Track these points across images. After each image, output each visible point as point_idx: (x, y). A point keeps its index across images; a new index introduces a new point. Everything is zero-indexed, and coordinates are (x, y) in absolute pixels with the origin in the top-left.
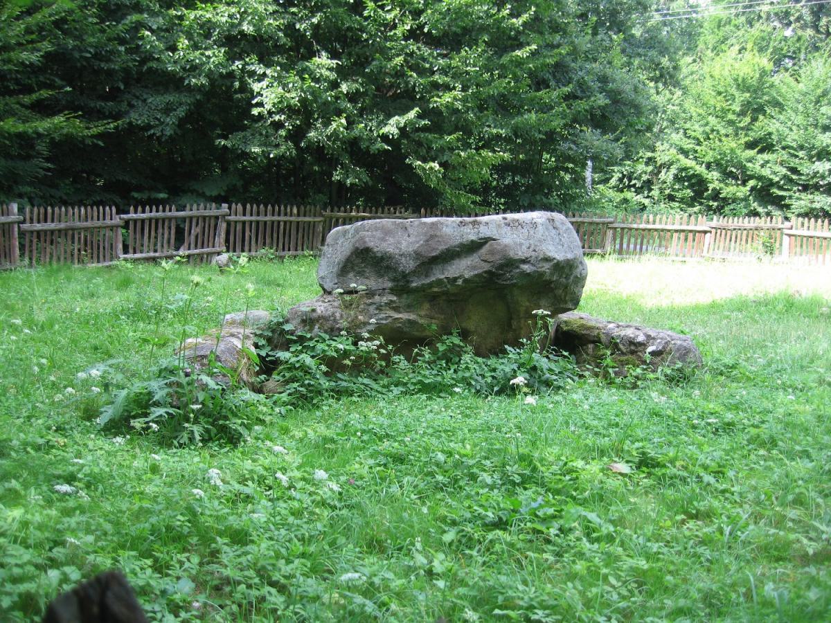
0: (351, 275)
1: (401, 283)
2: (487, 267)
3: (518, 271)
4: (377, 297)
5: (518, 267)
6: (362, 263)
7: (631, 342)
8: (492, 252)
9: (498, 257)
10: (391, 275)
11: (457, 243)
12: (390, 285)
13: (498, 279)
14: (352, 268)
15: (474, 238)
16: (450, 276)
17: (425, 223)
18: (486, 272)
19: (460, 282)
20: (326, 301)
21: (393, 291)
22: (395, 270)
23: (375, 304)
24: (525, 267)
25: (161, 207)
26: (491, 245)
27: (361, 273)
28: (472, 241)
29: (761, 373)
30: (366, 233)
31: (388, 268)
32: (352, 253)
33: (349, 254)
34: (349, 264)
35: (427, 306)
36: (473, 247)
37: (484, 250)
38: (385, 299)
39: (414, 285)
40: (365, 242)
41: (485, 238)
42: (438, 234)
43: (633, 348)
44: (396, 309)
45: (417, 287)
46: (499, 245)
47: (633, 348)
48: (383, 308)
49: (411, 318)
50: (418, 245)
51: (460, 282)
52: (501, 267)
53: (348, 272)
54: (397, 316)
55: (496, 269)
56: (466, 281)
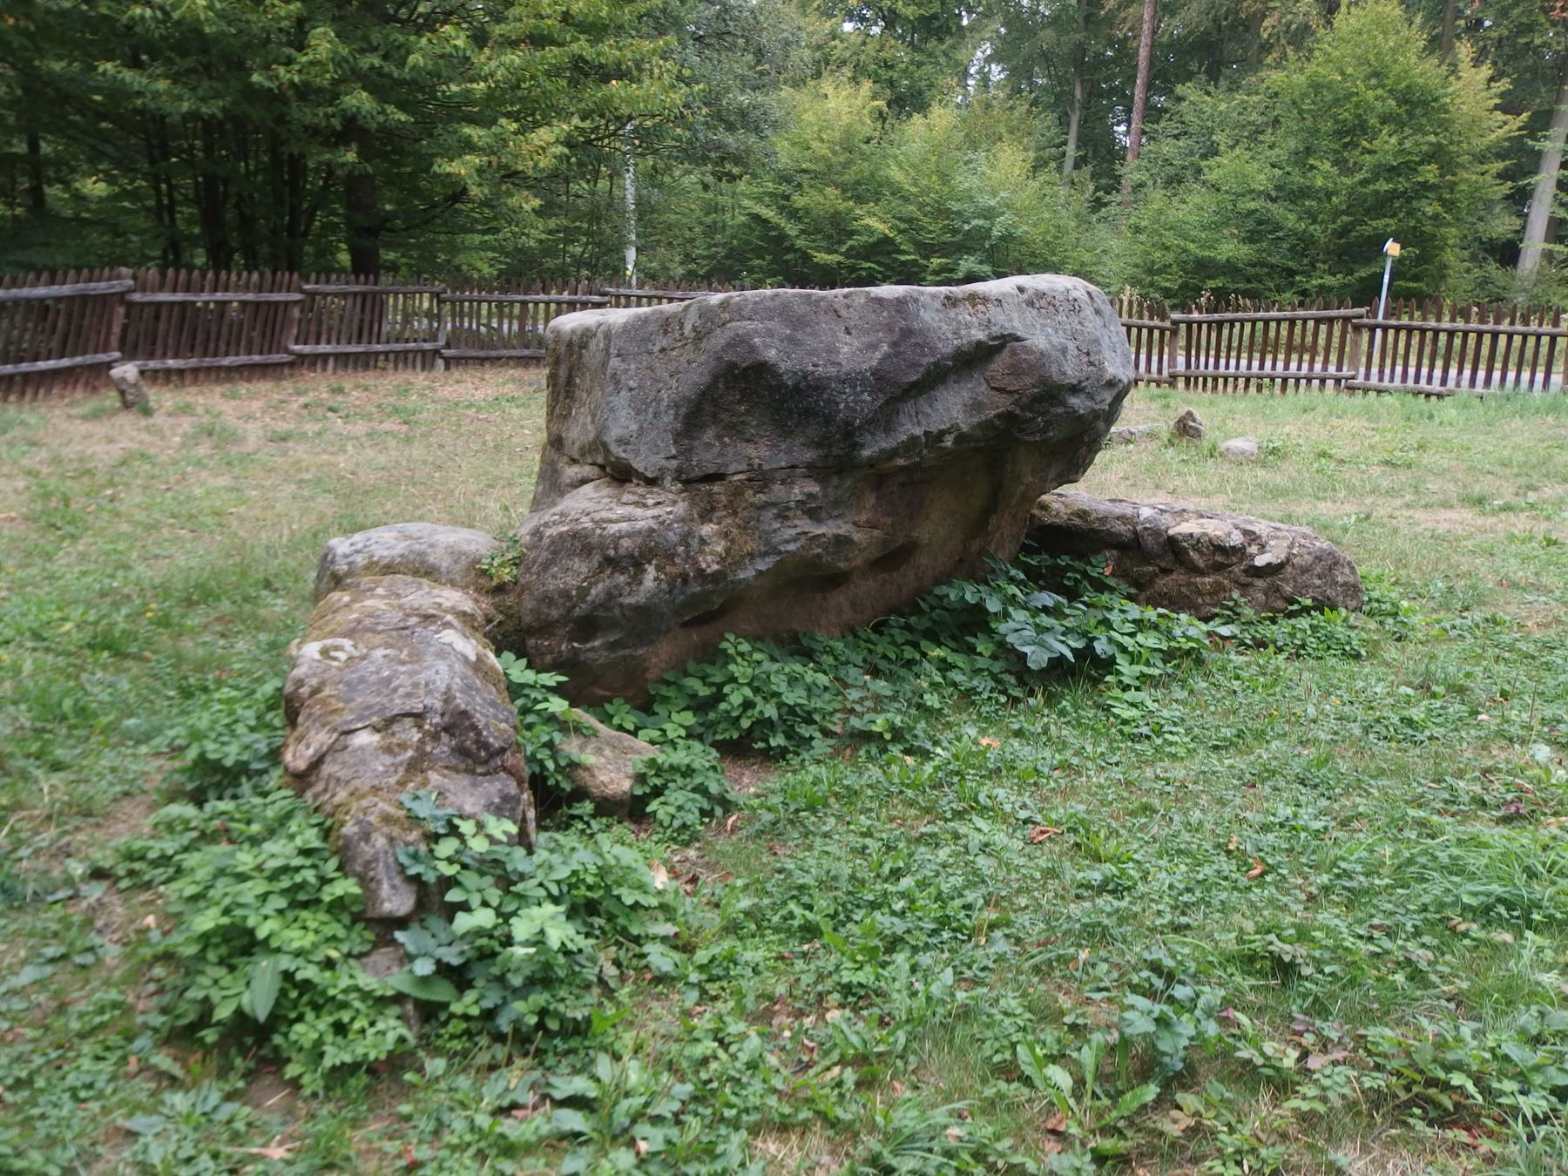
0: (709, 435)
1: (835, 451)
2: (1003, 403)
3: (1060, 410)
4: (777, 487)
5: (1063, 404)
6: (740, 402)
7: (1219, 548)
8: (1015, 370)
9: (1028, 380)
10: (813, 431)
11: (949, 350)
12: (809, 455)
13: (1022, 431)
14: (714, 416)
15: (980, 335)
16: (934, 429)
17: (879, 301)
18: (999, 416)
19: (948, 442)
20: (650, 502)
21: (815, 471)
22: (828, 420)
23: (774, 505)
24: (1075, 401)
25: (372, 277)
26: (1014, 353)
27: (735, 430)
28: (979, 343)
29: (532, 555)
30: (749, 325)
31: (809, 413)
32: (715, 378)
33: (706, 379)
34: (708, 408)
35: (870, 500)
36: (974, 358)
37: (999, 365)
38: (797, 493)
39: (866, 453)
40: (753, 349)
41: (1003, 336)
42: (916, 326)
43: (1219, 558)
44: (813, 514)
45: (870, 458)
46: (1028, 351)
47: (1219, 558)
48: (790, 514)
49: (841, 532)
50: (878, 355)
51: (948, 442)
52: (1036, 399)
53: (702, 427)
54: (819, 532)
55: (1026, 408)
56: (961, 438)
